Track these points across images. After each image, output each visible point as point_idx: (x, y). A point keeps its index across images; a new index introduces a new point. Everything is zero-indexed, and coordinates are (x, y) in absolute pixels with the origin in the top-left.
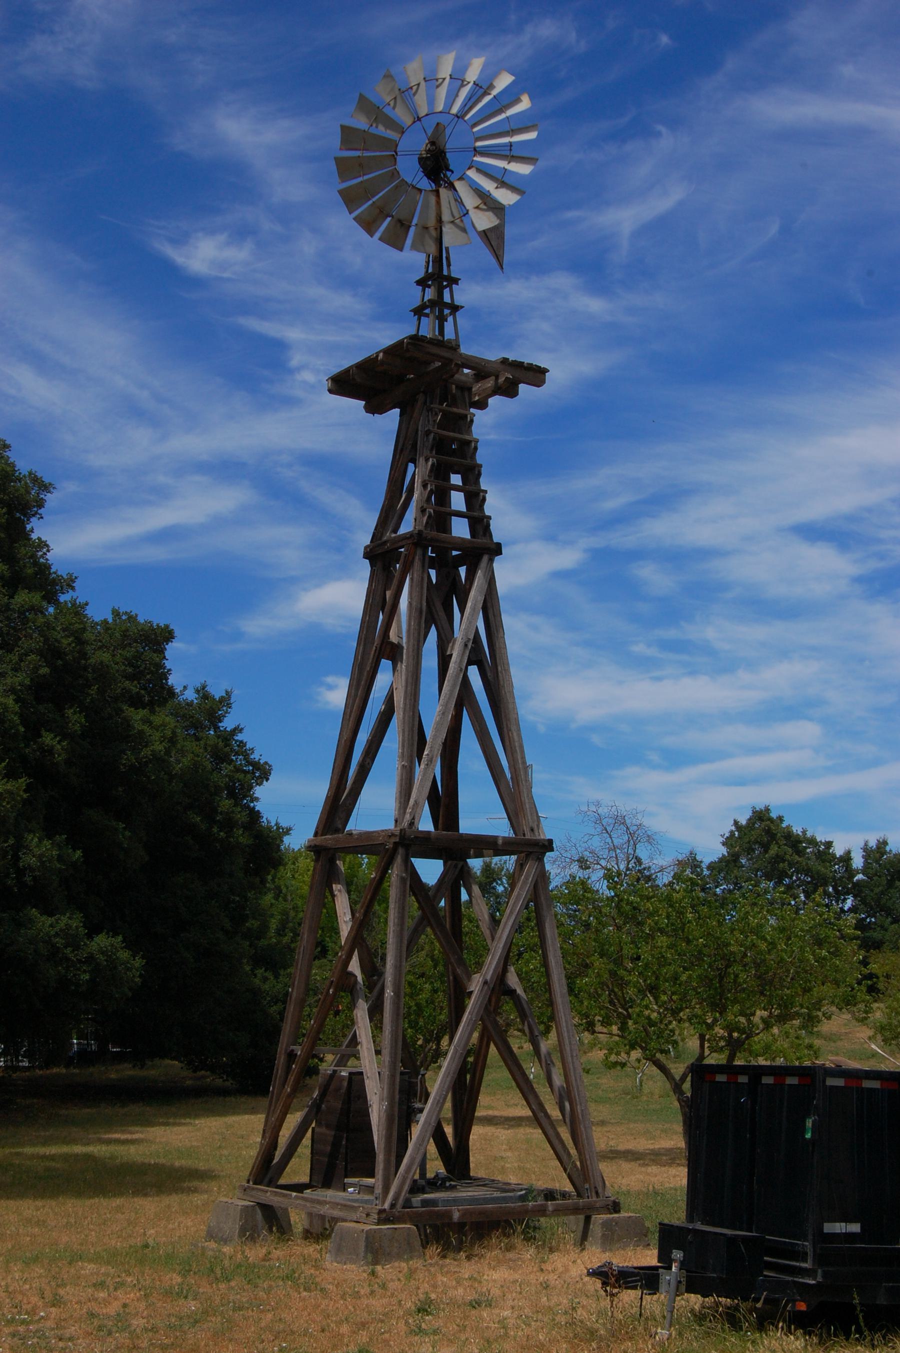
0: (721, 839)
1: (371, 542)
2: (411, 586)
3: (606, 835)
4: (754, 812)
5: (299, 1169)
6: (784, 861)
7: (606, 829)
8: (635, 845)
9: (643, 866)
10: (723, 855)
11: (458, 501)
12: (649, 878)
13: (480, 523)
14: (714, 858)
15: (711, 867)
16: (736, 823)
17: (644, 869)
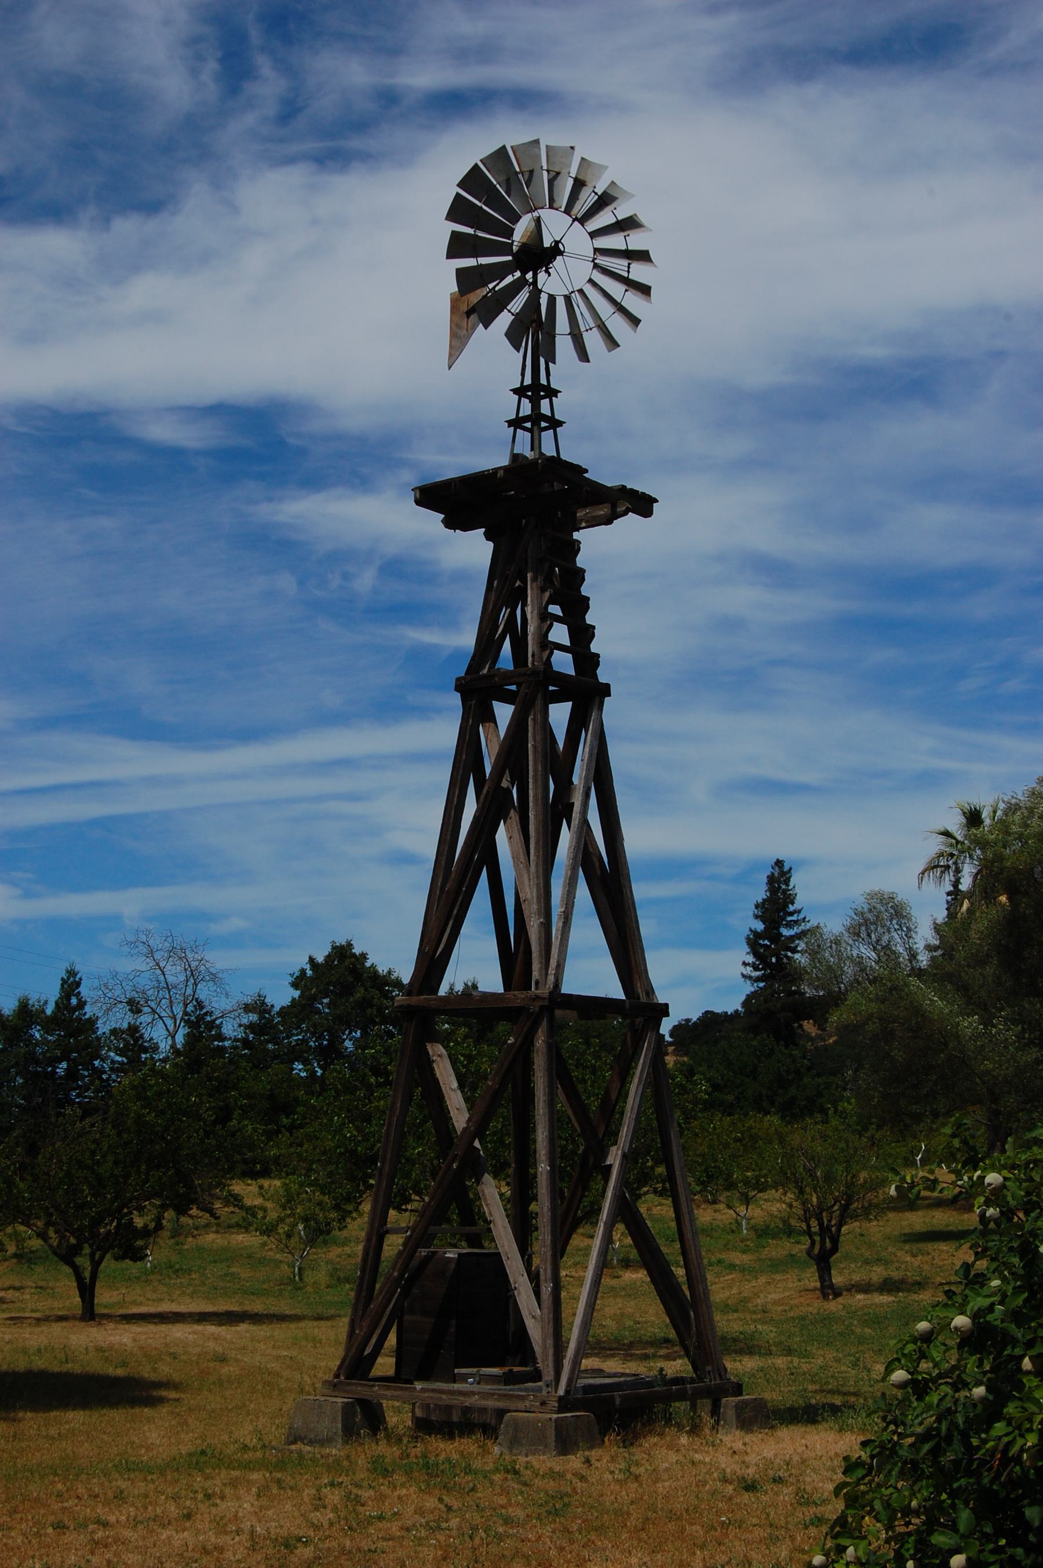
0: (291, 979)
1: (467, 673)
3: (158, 972)
4: (333, 948)
5: (385, 1365)
6: (371, 1006)
7: (158, 964)
8: (196, 984)
9: (204, 1011)
10: (294, 999)
12: (211, 1025)
14: (286, 1001)
15: (283, 1012)
16: (311, 960)
17: (206, 1014)
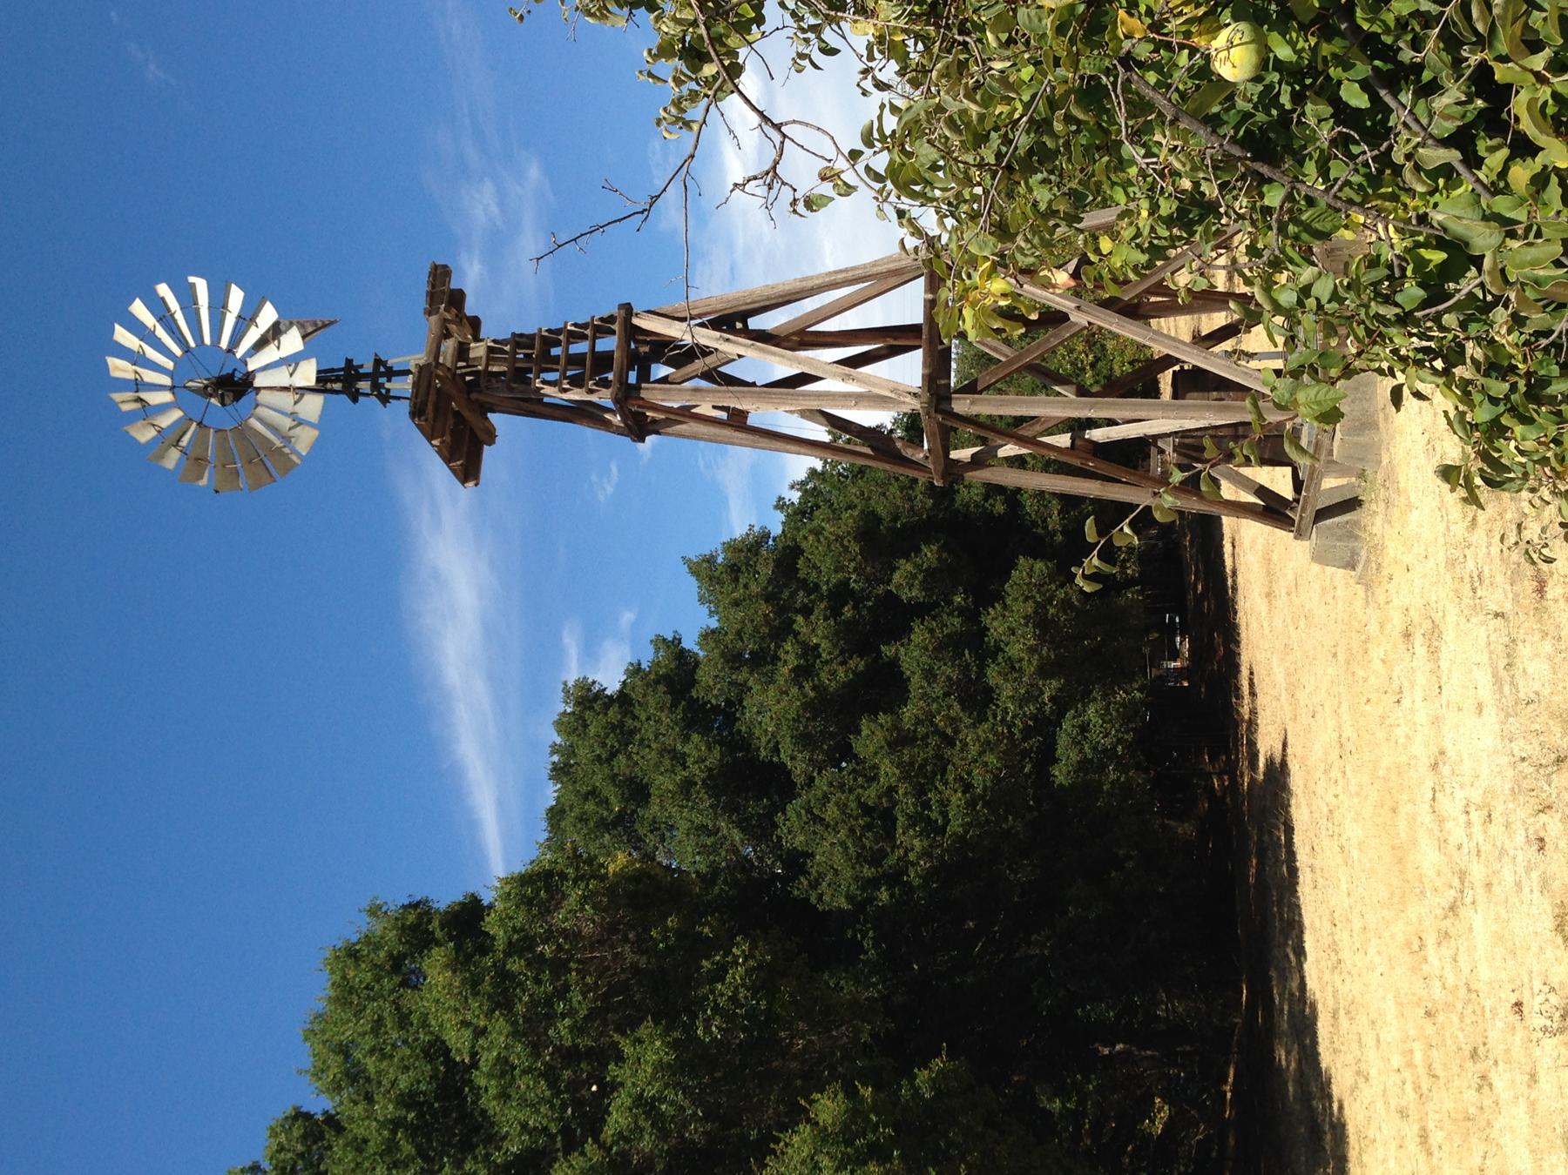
2: (836, 407)
5: (1279, 480)
11: (581, 347)
13: (602, 328)
